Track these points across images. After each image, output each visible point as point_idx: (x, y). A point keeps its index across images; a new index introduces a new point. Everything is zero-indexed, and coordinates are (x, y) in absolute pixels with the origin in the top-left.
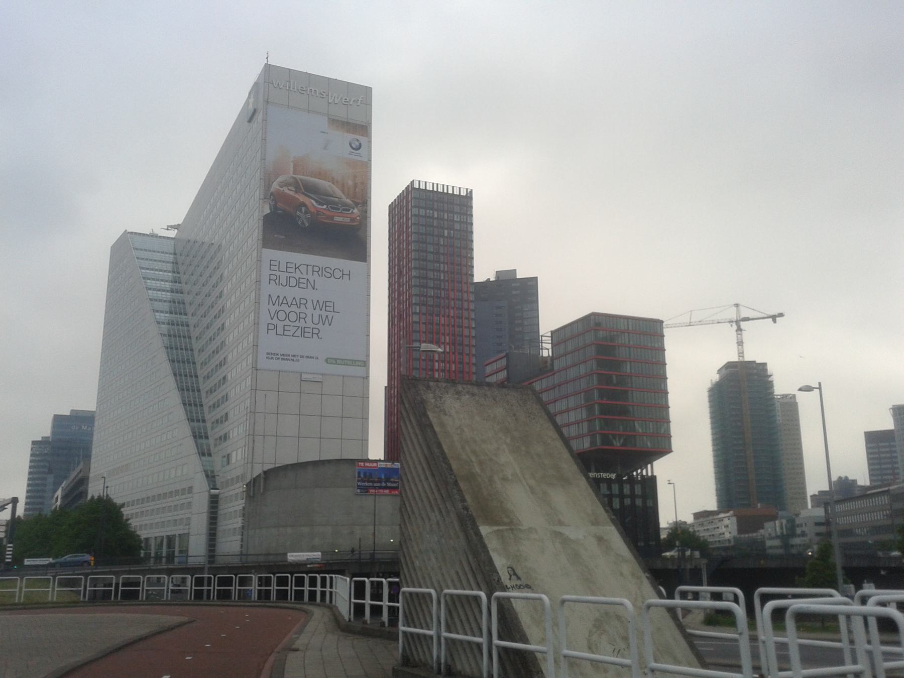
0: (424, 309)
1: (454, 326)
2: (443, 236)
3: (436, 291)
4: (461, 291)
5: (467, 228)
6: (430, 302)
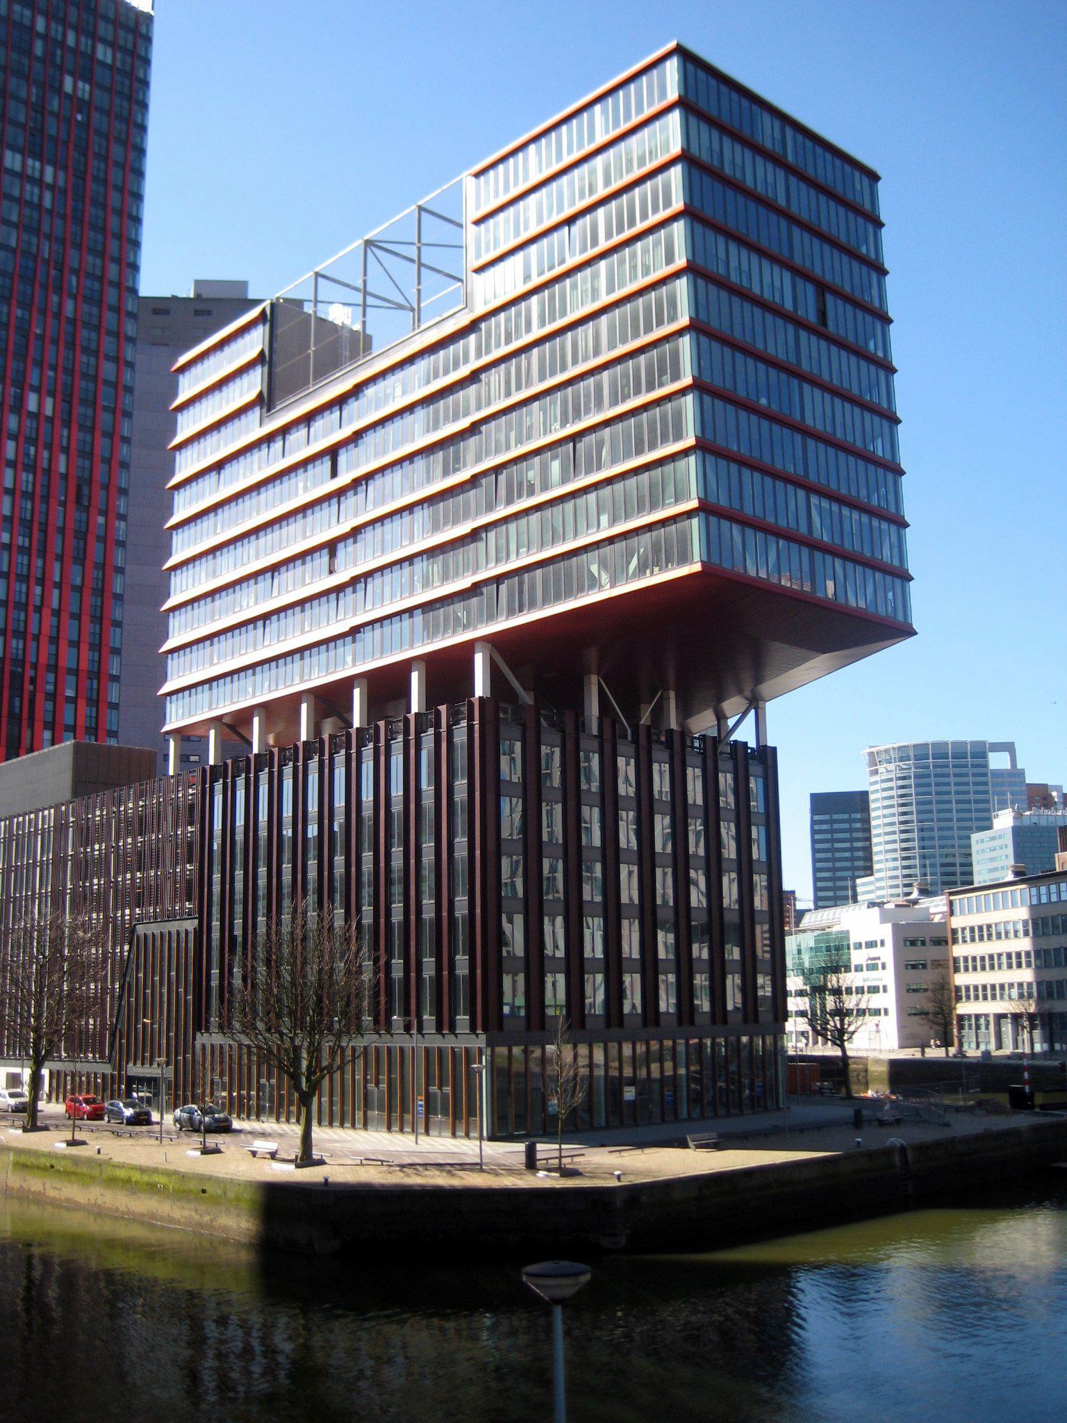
1: (57, 613)
3: (25, 237)
4: (102, 254)
5: (103, 269)
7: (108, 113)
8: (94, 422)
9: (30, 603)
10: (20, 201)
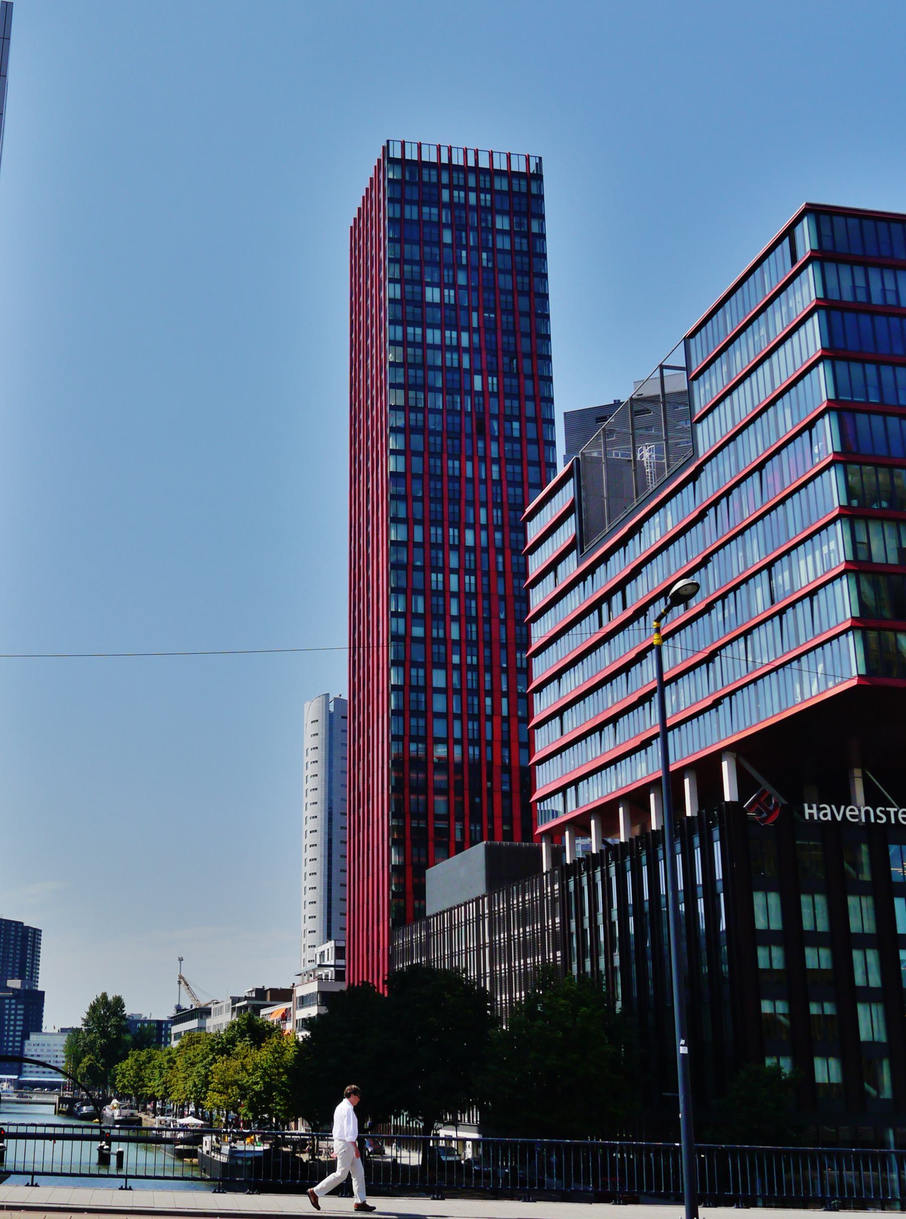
0: (417, 441)
2: (472, 392)
6: (434, 422)
7: (510, 272)
8: (514, 305)
9: (463, 497)
10: (443, 369)
